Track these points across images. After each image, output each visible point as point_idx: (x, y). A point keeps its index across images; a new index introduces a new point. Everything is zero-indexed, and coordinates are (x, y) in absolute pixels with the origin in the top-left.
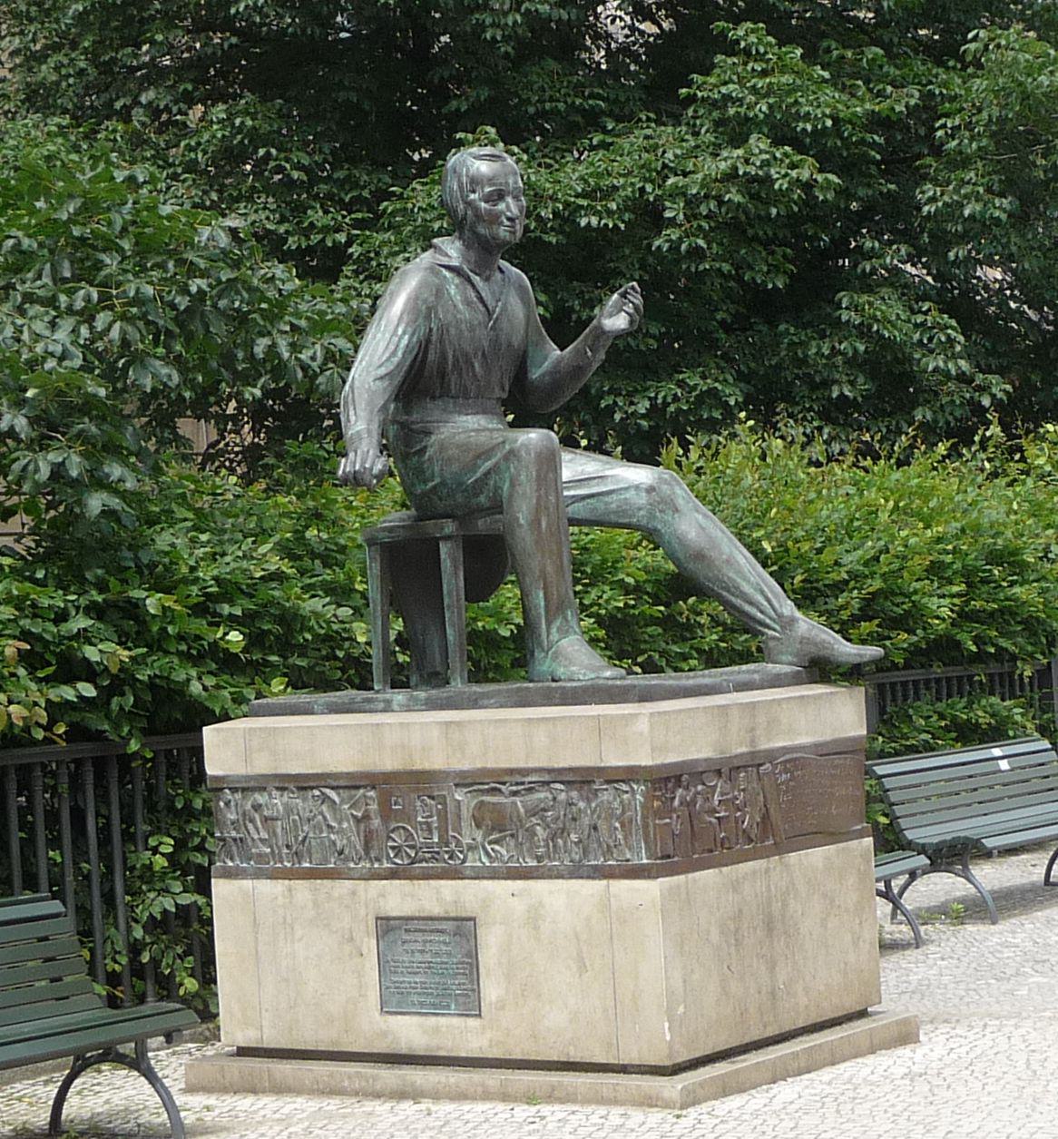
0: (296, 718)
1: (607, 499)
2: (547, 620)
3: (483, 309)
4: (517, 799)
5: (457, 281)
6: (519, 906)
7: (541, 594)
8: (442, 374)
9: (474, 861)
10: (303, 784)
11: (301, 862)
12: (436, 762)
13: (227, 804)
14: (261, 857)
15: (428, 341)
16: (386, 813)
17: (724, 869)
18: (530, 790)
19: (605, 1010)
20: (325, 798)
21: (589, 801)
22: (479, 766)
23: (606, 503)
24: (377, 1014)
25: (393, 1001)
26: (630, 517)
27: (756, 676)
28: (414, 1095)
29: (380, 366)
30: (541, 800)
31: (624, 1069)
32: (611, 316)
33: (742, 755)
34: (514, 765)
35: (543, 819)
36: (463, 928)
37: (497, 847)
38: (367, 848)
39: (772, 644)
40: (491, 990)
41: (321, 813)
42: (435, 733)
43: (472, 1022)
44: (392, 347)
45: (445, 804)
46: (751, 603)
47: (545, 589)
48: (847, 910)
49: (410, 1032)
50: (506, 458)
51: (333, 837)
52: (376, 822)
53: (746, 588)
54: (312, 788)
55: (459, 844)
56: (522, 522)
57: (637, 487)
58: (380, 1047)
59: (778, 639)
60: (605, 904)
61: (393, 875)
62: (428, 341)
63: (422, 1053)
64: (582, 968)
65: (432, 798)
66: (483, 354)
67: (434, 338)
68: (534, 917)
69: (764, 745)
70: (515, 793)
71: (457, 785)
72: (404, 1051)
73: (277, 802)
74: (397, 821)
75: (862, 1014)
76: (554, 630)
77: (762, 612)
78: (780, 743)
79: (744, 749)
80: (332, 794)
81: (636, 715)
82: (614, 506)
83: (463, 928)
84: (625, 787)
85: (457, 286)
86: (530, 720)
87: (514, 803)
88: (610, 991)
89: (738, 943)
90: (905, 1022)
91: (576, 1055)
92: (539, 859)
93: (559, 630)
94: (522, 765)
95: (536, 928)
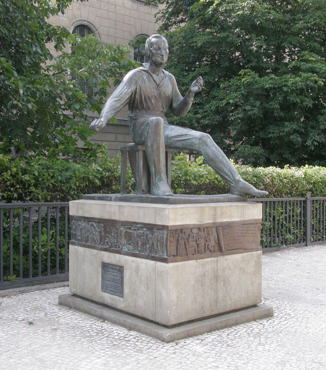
0: (211, 204)
1: (187, 141)
2: (155, 176)
3: (155, 84)
4: (135, 232)
5: (147, 74)
6: (134, 265)
7: (154, 168)
8: (141, 102)
9: (125, 249)
10: (88, 220)
11: (86, 243)
12: (116, 217)
13: (73, 223)
14: (79, 240)
15: (136, 92)
16: (106, 232)
17: (199, 261)
18: (138, 229)
19: (153, 303)
20: (92, 225)
21: (152, 235)
22: (127, 220)
23: (187, 143)
24: (100, 291)
25: (104, 289)
26: (193, 147)
27: (222, 198)
28: (104, 319)
29: (116, 97)
30: (140, 233)
31: (158, 324)
32: (193, 87)
33: (209, 223)
34: (134, 221)
35: (141, 239)
36: (120, 269)
37: (130, 246)
38: (101, 241)
39: (232, 188)
40: (126, 290)
41: (92, 229)
42: (117, 208)
43: (121, 299)
44: (121, 92)
45: (118, 230)
46: (227, 175)
47: (155, 166)
48: (250, 273)
49: (108, 298)
50: (146, 125)
51: (94, 236)
52: (103, 234)
53: (226, 170)
54: (90, 222)
55: (121, 244)
56: (149, 145)
57: (196, 138)
58: (100, 301)
59: (234, 187)
60: (154, 269)
61: (106, 250)
62: (136, 92)
63: (110, 305)
64: (148, 288)
65: (115, 228)
66: (155, 97)
67: (138, 90)
68: (137, 268)
69: (219, 220)
70: (135, 230)
71: (122, 225)
72: (106, 303)
73: (83, 224)
74: (107, 235)
75: (255, 306)
76: (157, 179)
77: (230, 178)
78: (225, 220)
79: (210, 221)
80: (94, 224)
81: (166, 208)
82: (189, 143)
83: (120, 269)
84: (161, 232)
85: (146, 76)
86: (139, 207)
87: (134, 233)
88: (154, 298)
89: (202, 285)
90: (269, 310)
91: (145, 315)
92: (139, 251)
93: (158, 179)
94: (136, 221)
95: (137, 273)
